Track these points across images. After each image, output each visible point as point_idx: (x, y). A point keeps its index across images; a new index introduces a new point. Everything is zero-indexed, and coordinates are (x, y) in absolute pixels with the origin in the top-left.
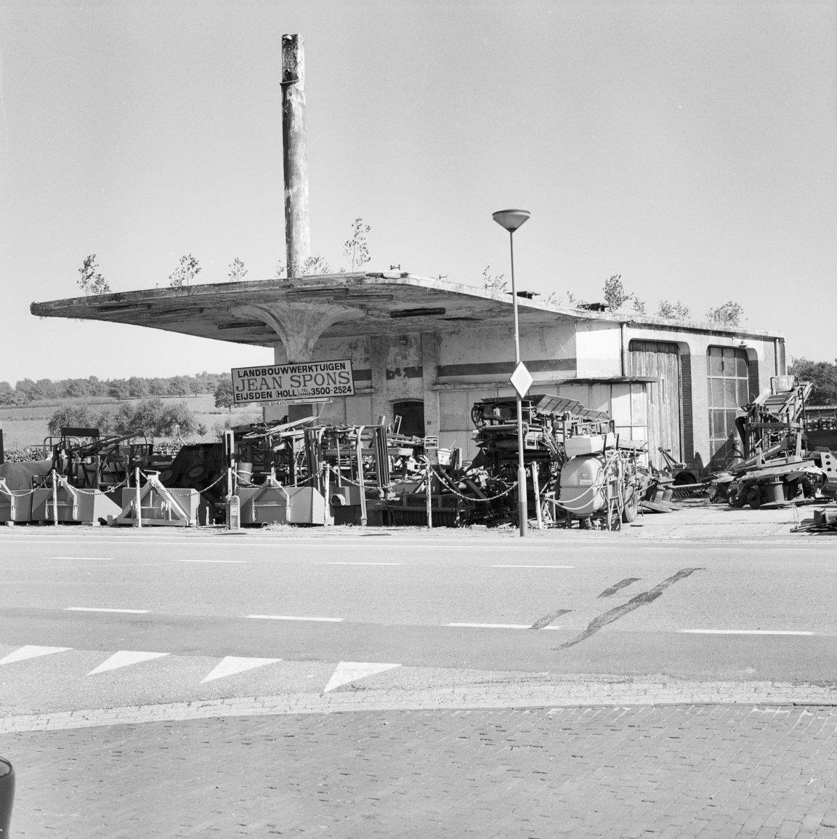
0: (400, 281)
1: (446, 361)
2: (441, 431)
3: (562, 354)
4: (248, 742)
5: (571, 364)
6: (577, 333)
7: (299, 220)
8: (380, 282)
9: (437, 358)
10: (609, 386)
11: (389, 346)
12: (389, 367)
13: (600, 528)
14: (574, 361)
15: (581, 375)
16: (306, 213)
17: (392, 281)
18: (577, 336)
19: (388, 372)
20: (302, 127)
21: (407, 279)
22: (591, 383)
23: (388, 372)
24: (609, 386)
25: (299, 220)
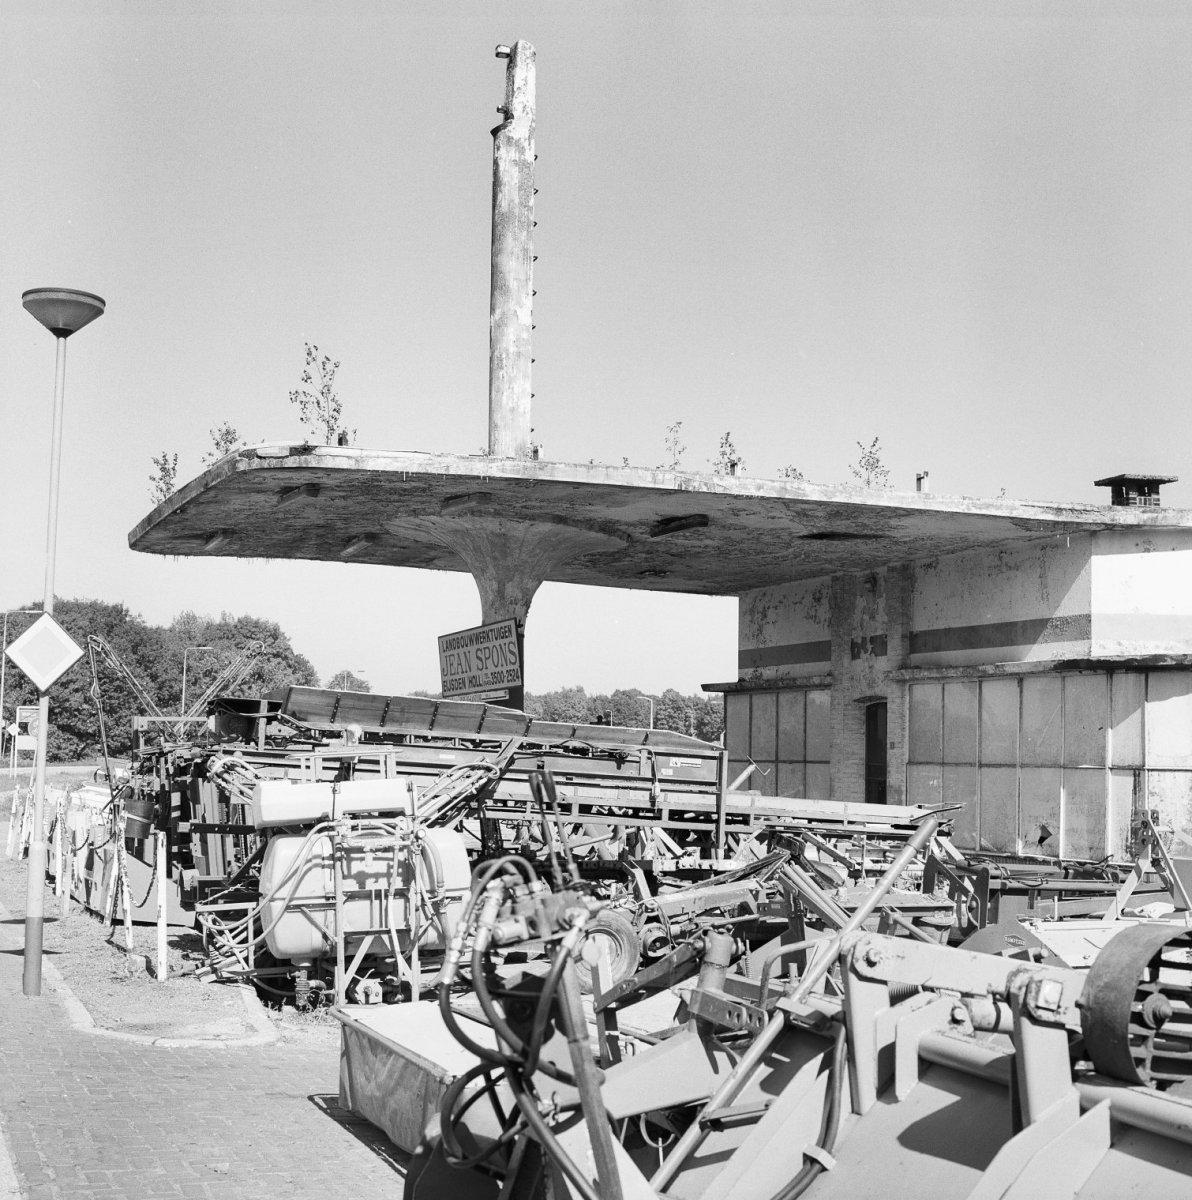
0: (291, 462)
1: (921, 624)
2: (910, 763)
3: (1067, 608)
4: (32, 985)
5: (1081, 626)
6: (1092, 557)
7: (502, 368)
8: (254, 466)
9: (907, 616)
10: (1143, 677)
11: (855, 598)
12: (854, 634)
13: (876, 920)
14: (1088, 618)
15: (1102, 647)
16: (519, 354)
17: (274, 463)
18: (1093, 562)
19: (853, 645)
20: (517, 201)
21: (309, 457)
22: (1109, 668)
23: (853, 645)
24: (1143, 677)
25: (502, 368)
